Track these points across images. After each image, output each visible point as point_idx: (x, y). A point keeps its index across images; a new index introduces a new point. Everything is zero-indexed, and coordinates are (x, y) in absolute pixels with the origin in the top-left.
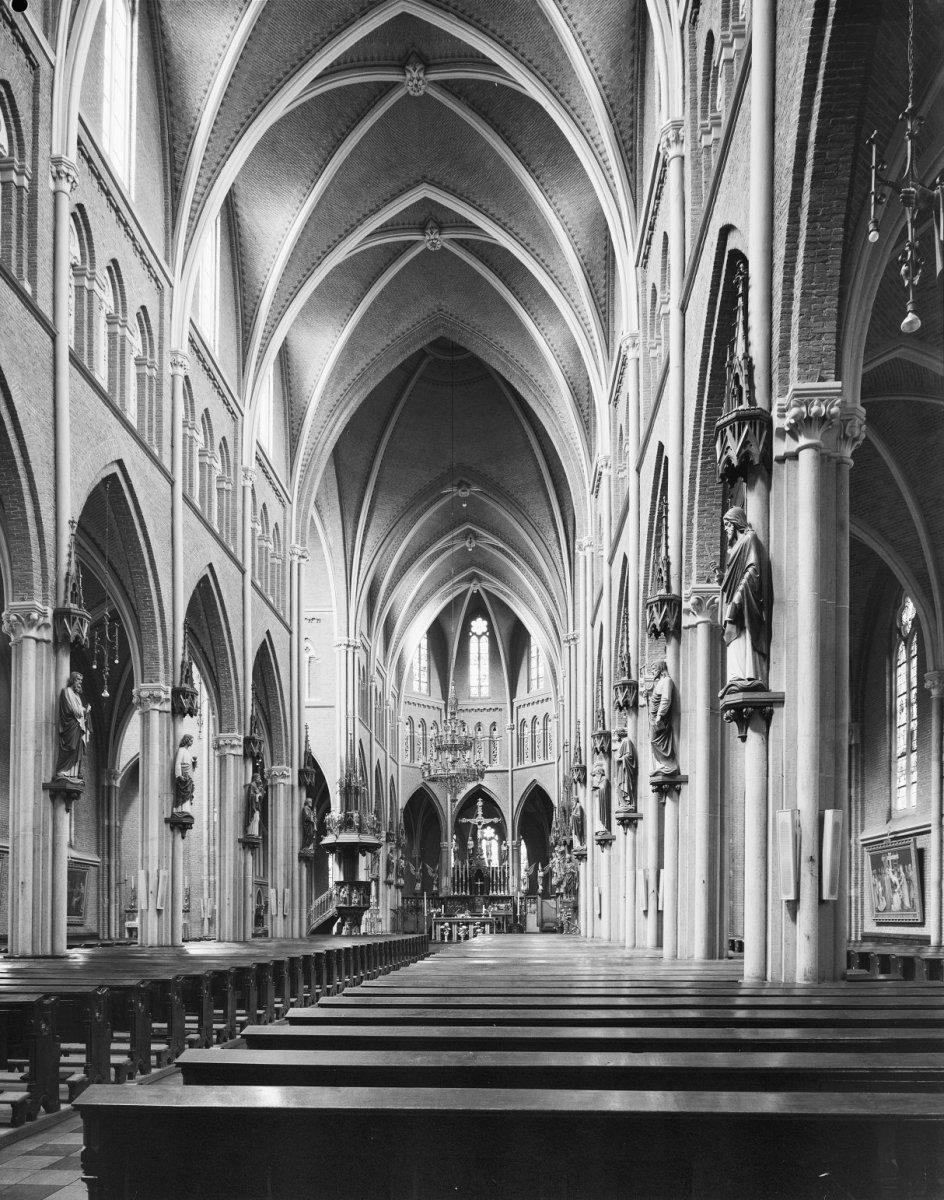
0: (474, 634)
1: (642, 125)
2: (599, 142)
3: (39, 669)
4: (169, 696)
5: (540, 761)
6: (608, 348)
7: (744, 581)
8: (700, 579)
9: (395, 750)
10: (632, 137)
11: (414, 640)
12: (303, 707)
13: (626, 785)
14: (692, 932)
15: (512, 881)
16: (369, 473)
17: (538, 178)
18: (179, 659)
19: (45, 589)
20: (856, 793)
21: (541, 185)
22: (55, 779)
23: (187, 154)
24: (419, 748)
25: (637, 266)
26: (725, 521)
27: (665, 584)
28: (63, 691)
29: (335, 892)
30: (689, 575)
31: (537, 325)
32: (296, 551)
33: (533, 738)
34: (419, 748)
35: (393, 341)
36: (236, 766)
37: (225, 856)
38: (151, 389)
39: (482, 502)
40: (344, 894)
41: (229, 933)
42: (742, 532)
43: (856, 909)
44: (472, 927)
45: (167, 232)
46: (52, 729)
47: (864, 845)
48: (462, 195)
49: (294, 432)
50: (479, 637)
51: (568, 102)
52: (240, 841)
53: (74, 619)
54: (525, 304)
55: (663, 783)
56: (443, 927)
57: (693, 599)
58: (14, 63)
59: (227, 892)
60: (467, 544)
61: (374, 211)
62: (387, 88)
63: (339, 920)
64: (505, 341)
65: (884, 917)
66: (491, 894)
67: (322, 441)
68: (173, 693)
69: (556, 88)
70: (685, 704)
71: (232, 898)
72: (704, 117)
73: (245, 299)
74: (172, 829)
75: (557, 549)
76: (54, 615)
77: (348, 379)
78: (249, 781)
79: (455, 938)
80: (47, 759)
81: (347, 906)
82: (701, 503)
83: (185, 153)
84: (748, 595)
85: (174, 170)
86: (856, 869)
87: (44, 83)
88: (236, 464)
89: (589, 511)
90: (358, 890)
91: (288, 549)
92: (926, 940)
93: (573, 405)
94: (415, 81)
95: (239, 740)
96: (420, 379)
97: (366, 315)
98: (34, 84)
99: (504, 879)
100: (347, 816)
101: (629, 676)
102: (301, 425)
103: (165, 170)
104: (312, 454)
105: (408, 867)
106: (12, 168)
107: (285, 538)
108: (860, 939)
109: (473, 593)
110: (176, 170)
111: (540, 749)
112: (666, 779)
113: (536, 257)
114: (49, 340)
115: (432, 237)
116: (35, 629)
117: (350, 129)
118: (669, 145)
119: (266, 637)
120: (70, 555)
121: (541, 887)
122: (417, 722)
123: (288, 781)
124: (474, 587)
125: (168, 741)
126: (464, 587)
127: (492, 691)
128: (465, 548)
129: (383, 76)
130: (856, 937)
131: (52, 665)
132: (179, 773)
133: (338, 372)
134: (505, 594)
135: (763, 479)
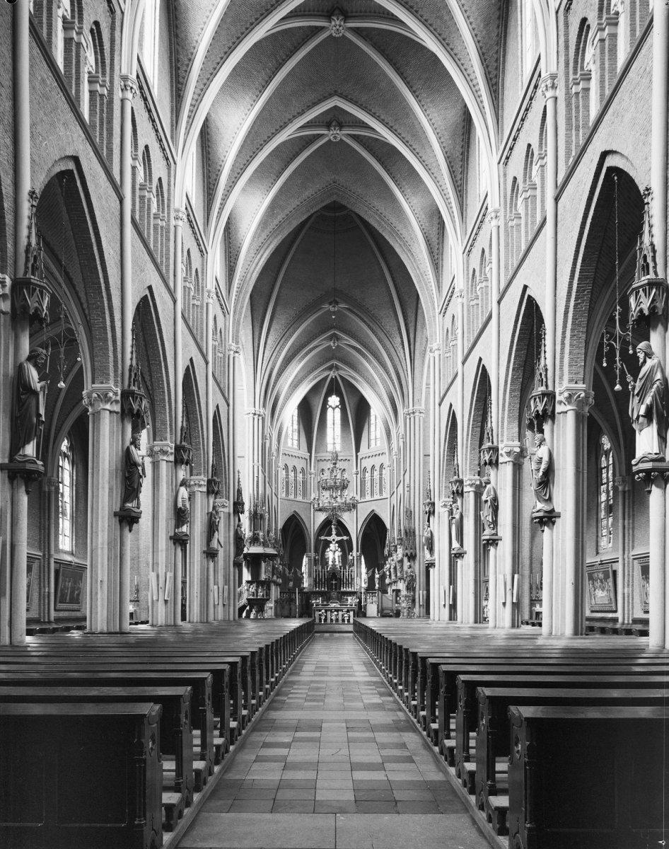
0: (330, 406)
1: (504, 68)
2: (473, 78)
3: (112, 432)
4: (173, 451)
5: (376, 497)
6: (462, 215)
7: (653, 390)
8: (571, 381)
9: (277, 488)
10: (496, 76)
11: (290, 414)
12: (236, 457)
13: (490, 517)
14: (564, 617)
15: (356, 580)
16: (271, 293)
17: (417, 97)
18: (128, 363)
19: (116, 376)
20: (629, 523)
21: (419, 102)
22: (122, 508)
23: (188, 72)
24: (292, 490)
25: (499, 163)
26: (638, 350)
27: (544, 384)
28: (128, 448)
29: (246, 588)
30: (561, 378)
31: (404, 196)
32: (232, 348)
33: (372, 480)
34: (292, 490)
35: (302, 203)
36: (202, 500)
37: (194, 563)
38: (162, 236)
39: (345, 315)
40: (252, 589)
41: (197, 616)
42: (650, 358)
43: (628, 602)
44: (340, 613)
45: (172, 126)
46: (120, 474)
47: (634, 559)
48: (362, 105)
49: (232, 264)
50: (334, 409)
51: (452, 49)
52: (204, 552)
53: (137, 398)
54: (396, 181)
55: (544, 517)
56: (320, 613)
57: (566, 394)
58: (102, 9)
59: (196, 587)
60: (332, 344)
61: (301, 113)
62: (316, 30)
63: (248, 608)
64: (379, 205)
65: (594, 609)
66: (342, 590)
67: (251, 271)
68: (175, 448)
69: (444, 40)
70: (558, 465)
71: (199, 592)
72: (575, 72)
73: (209, 172)
74: (174, 544)
75: (402, 350)
76: (122, 394)
77: (270, 228)
78: (211, 510)
79: (329, 621)
80: (117, 495)
81: (255, 597)
82: (572, 330)
83: (186, 71)
84: (656, 399)
85: (178, 82)
86: (629, 575)
87: (118, 24)
88: (203, 287)
89: (438, 326)
90: (263, 587)
91: (227, 346)
92: (615, 620)
93: (428, 252)
94: (338, 27)
95: (204, 481)
96: (310, 228)
97: (285, 183)
98: (112, 24)
99: (351, 579)
100: (254, 534)
101: (493, 443)
102: (236, 259)
103: (171, 82)
104: (243, 279)
105: (284, 570)
106: (98, 82)
107: (225, 338)
108: (631, 622)
109: (332, 378)
110: (179, 83)
111: (377, 489)
112: (546, 514)
113: (413, 151)
114: (118, 202)
115: (335, 132)
116: (109, 404)
117: (289, 57)
118: (547, 89)
119: (189, 363)
120: (132, 353)
121: (377, 586)
122: (290, 468)
123: (226, 510)
124: (332, 374)
125: (172, 482)
126: (326, 374)
127: (343, 447)
128: (330, 347)
129: (316, 23)
130: (628, 621)
131: (120, 427)
132: (180, 505)
133: (264, 224)
134: (355, 379)
135: (662, 324)
